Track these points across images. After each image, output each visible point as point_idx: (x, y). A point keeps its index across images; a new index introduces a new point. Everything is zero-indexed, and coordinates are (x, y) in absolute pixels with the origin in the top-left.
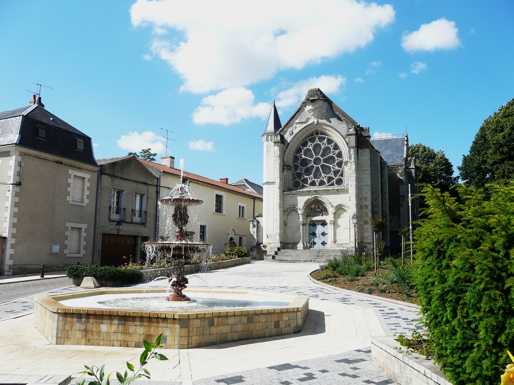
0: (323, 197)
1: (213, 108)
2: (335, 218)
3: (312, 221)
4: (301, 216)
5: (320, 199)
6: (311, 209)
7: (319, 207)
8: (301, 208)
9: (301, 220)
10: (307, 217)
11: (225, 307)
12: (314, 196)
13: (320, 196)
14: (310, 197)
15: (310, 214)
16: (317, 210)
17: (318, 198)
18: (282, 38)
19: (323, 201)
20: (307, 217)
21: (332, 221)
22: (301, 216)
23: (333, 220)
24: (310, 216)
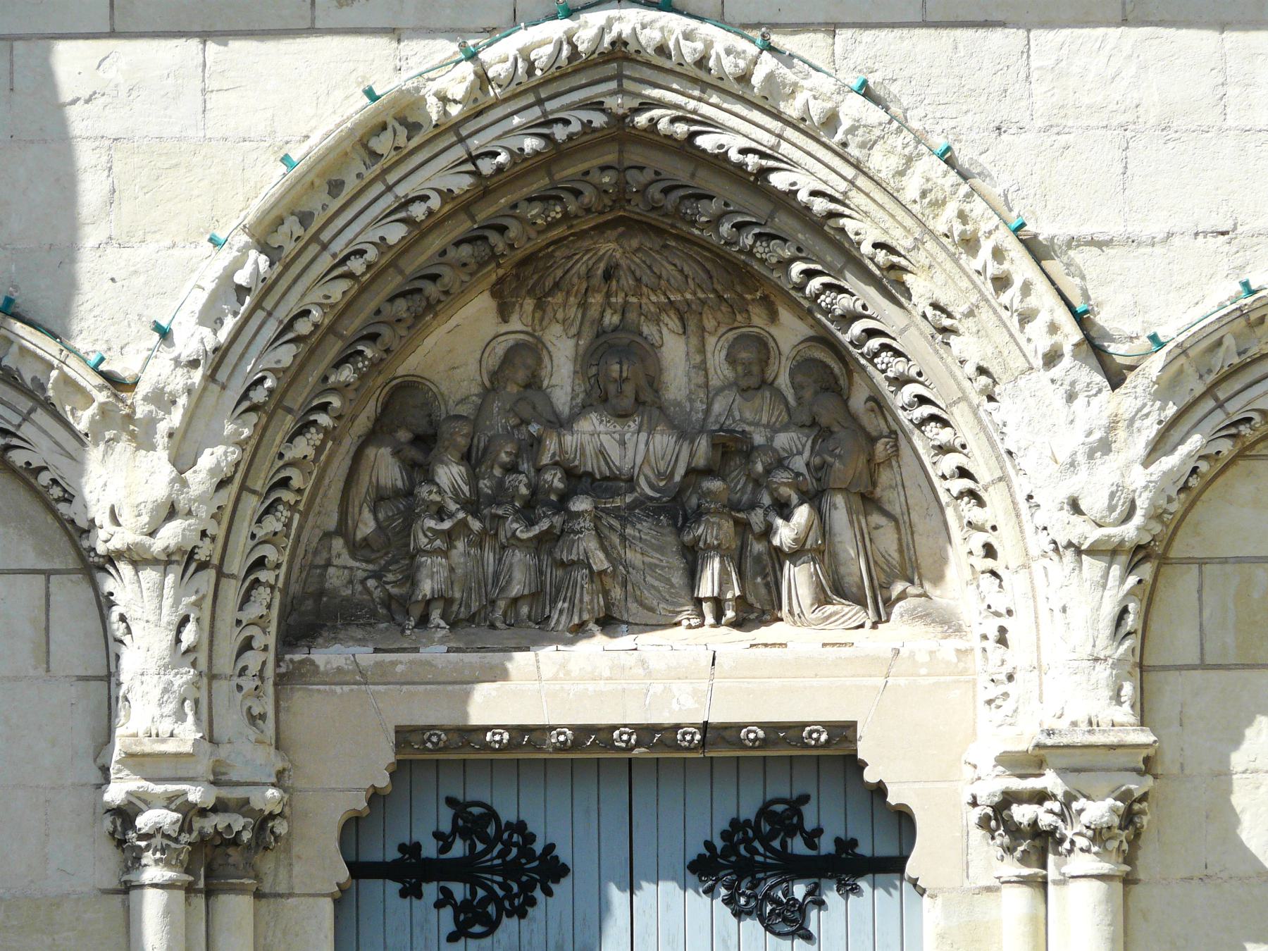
0: (822, 69)
1: (909, 360)
2: (1144, 672)
3: (436, 755)
4: (146, 612)
5: (732, 134)
6: (409, 418)
7: (620, 373)
8: (158, 371)
9: (152, 709)
10: (307, 620)
11: (1164, 459)
12: (543, 39)
13: (725, 47)
14: (435, 72)
15: (394, 550)
16: (596, 438)
17: (666, 109)
18: (1083, 506)
19: (804, 175)
20: (307, 620)
21: (1081, 762)
22: (146, 612)
23: (1117, 722)
24: (396, 614)
